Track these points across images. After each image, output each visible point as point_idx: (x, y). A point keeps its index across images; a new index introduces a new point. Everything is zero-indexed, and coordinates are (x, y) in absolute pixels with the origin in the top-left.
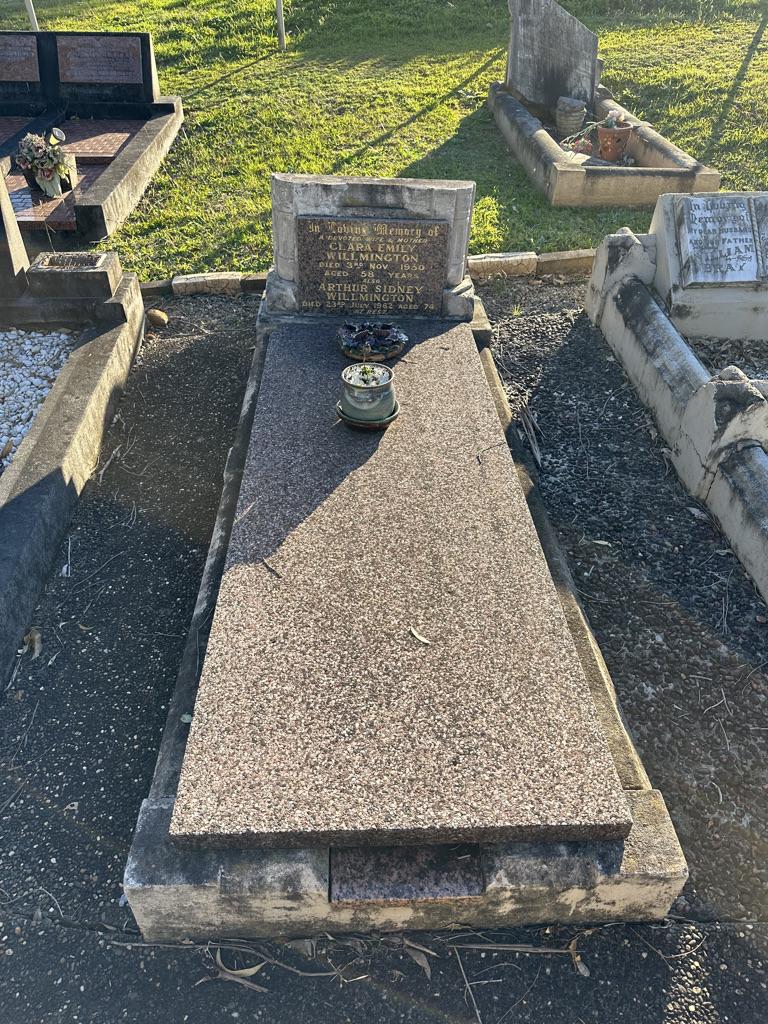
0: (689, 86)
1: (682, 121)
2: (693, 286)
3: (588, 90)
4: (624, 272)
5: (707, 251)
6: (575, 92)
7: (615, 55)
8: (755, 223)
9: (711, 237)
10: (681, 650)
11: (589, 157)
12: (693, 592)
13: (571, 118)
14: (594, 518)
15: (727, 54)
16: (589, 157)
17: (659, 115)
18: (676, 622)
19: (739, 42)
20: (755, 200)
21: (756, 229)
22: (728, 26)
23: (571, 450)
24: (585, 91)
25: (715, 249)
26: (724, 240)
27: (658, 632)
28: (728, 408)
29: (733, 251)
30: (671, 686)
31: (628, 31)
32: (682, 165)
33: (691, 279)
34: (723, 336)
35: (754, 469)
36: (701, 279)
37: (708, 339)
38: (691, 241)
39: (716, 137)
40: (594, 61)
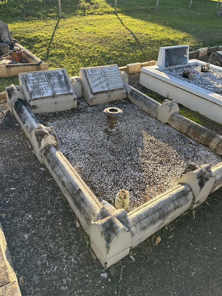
0: (39, 38)
1: (39, 48)
2: (34, 99)
3: (9, 40)
4: (14, 98)
5: (36, 89)
6: (5, 41)
7: (18, 30)
8: (48, 79)
9: (36, 84)
10: (37, 217)
11: (11, 61)
12: (41, 196)
13: (5, 49)
14: (10, 181)
15: (50, 29)
16: (11, 61)
17: (32, 47)
18: (35, 208)
19: (52, 26)
20: (46, 73)
21: (48, 81)
22: (50, 21)
23: (4, 158)
24: (8, 41)
25: (38, 88)
26: (40, 85)
27: (29, 214)
28: (40, 138)
29: (43, 88)
30: (33, 232)
31: (22, 23)
32: (37, 62)
33: (33, 98)
34: (50, 112)
35: (51, 153)
36: (36, 97)
37: (45, 113)
38: (30, 87)
39: (48, 52)
40: (8, 32)
